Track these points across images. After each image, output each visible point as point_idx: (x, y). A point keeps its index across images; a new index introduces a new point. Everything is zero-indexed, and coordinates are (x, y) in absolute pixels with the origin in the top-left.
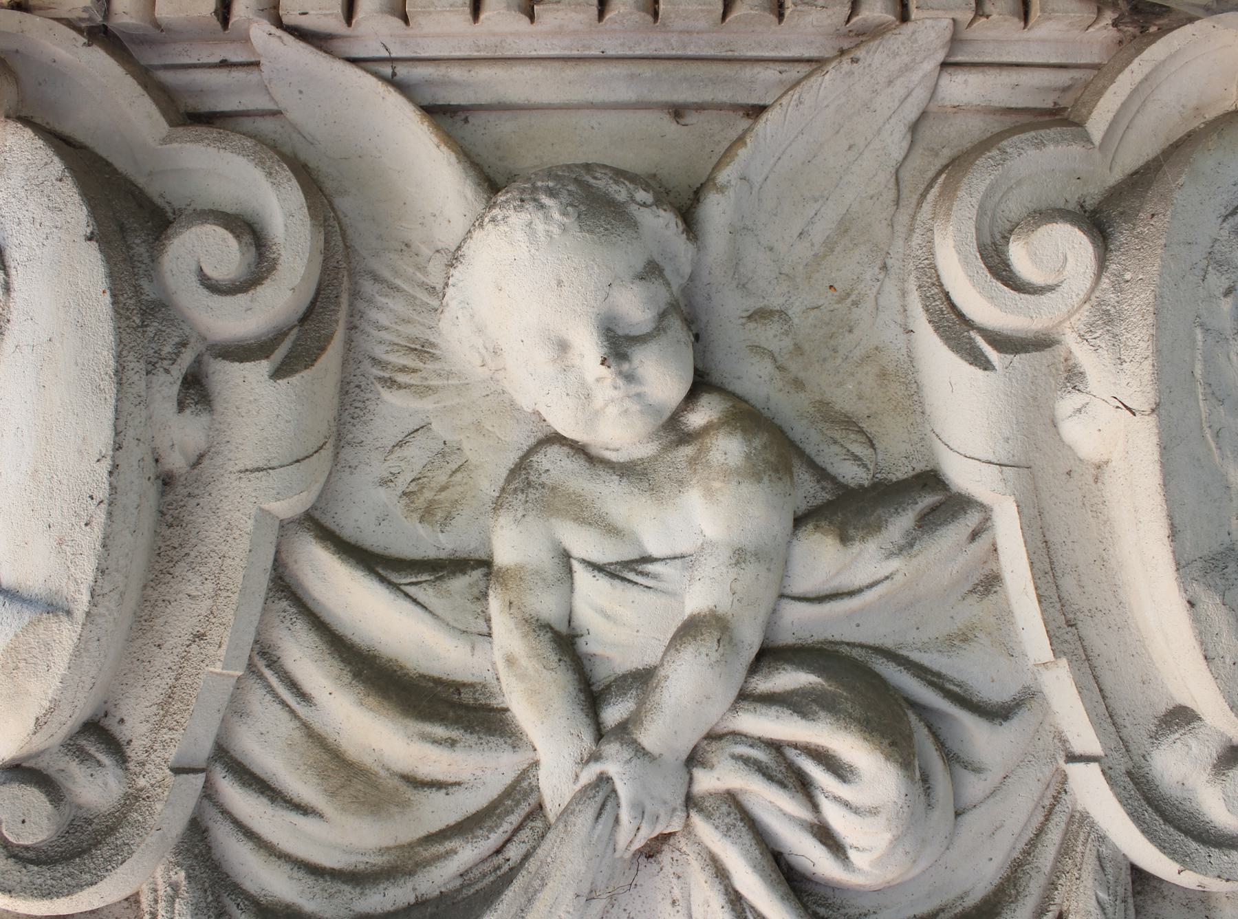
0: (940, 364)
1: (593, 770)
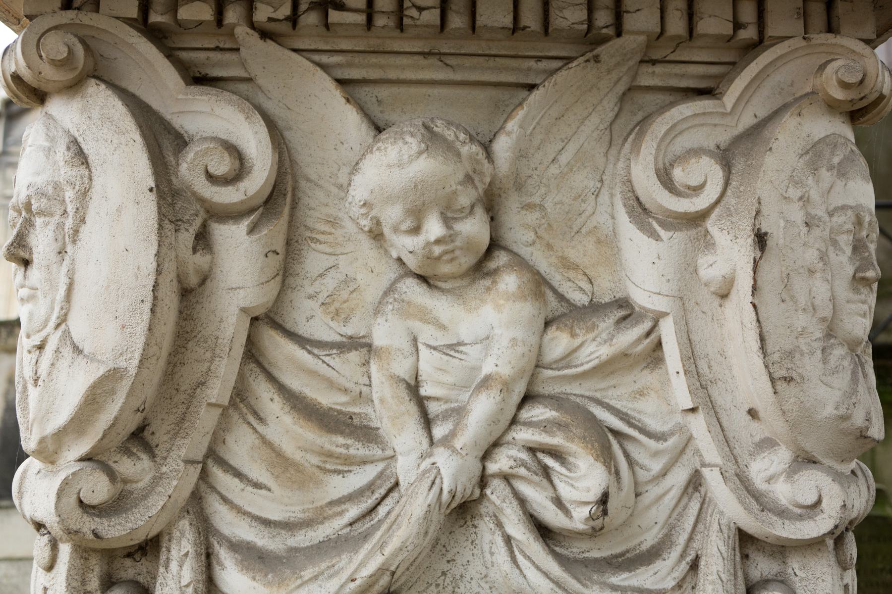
0: (630, 235)
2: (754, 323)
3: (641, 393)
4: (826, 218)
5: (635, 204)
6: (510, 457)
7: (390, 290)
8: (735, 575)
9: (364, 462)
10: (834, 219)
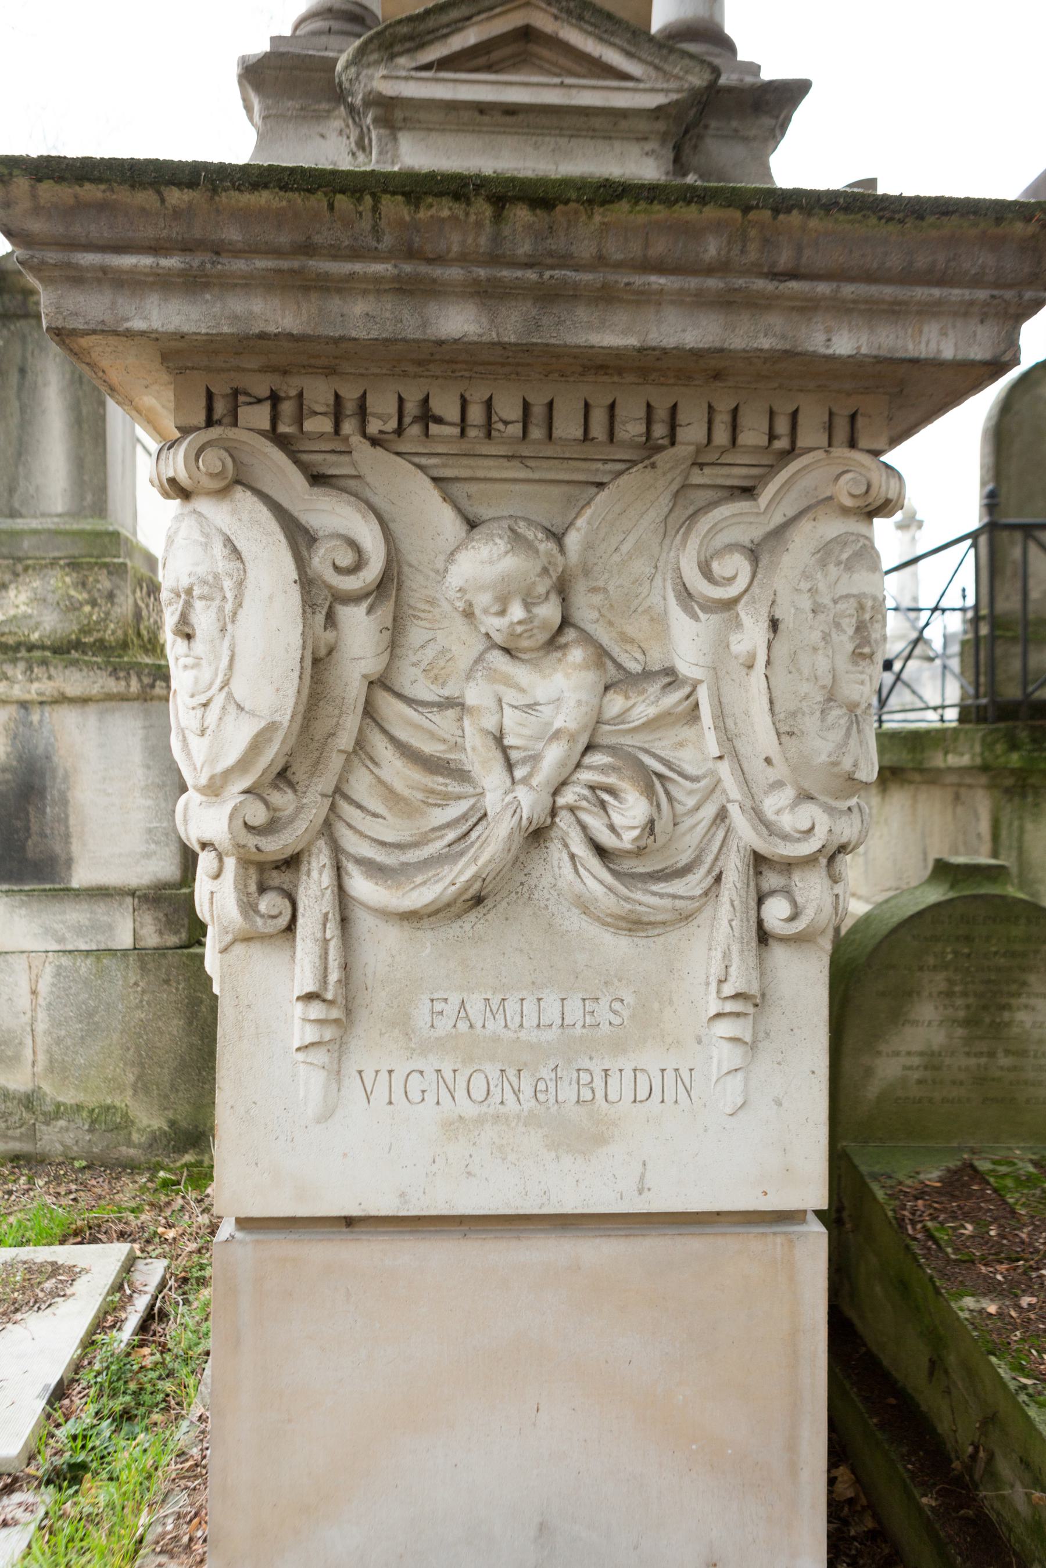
1: (509, 798)
2: (766, 690)
3: (681, 745)
4: (831, 605)
5: (682, 589)
6: (575, 793)
7: (479, 659)
8: (748, 885)
9: (459, 797)
10: (838, 606)
